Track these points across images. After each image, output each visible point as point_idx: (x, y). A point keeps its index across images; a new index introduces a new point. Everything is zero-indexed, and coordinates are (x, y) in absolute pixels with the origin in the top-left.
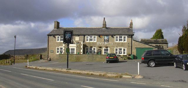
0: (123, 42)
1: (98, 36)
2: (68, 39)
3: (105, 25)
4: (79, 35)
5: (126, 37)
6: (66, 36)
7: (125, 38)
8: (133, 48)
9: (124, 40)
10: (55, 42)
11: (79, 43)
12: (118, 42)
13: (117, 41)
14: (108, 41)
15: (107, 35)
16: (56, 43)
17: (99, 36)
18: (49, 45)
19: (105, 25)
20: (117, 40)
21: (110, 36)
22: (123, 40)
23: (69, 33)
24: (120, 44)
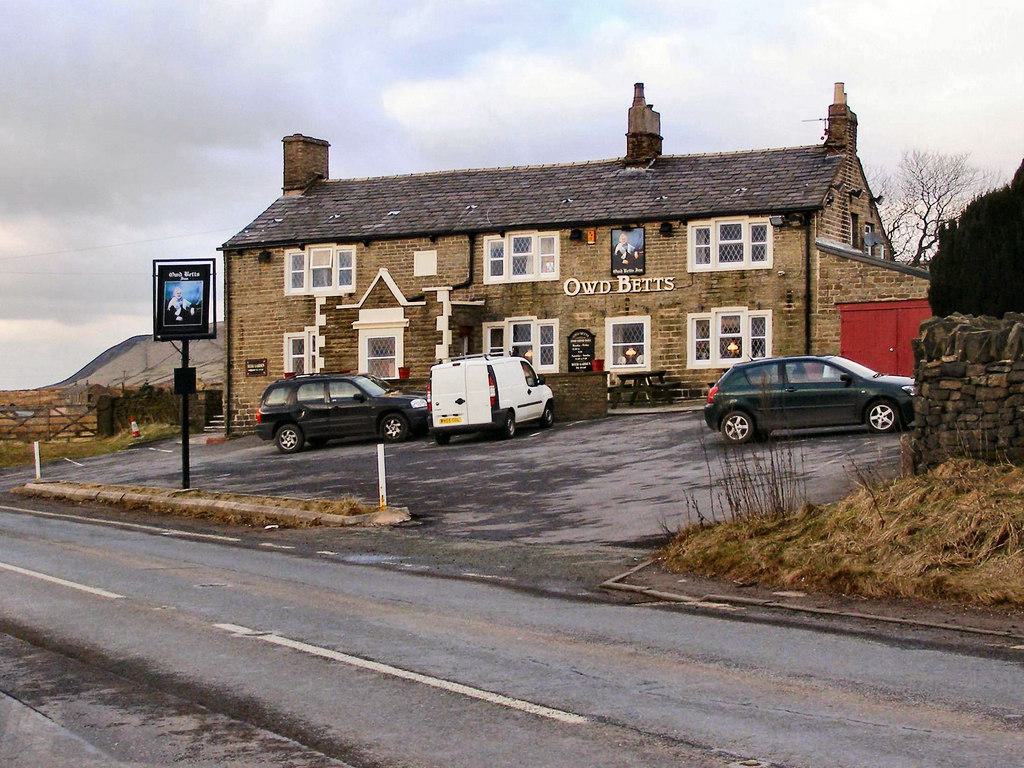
0: (747, 264)
1: (568, 233)
2: (184, 313)
3: (644, 141)
4: (434, 237)
5: (770, 230)
6: (170, 295)
7: (758, 233)
8: (817, 307)
9: (758, 253)
10: (274, 297)
11: (420, 298)
12: (715, 265)
13: (707, 260)
14: (638, 264)
15: (626, 225)
16: (287, 302)
17: (577, 232)
18: (235, 323)
19: (644, 141)
20: (707, 251)
21: (653, 228)
22: (747, 252)
23: (191, 279)
24: (728, 284)
